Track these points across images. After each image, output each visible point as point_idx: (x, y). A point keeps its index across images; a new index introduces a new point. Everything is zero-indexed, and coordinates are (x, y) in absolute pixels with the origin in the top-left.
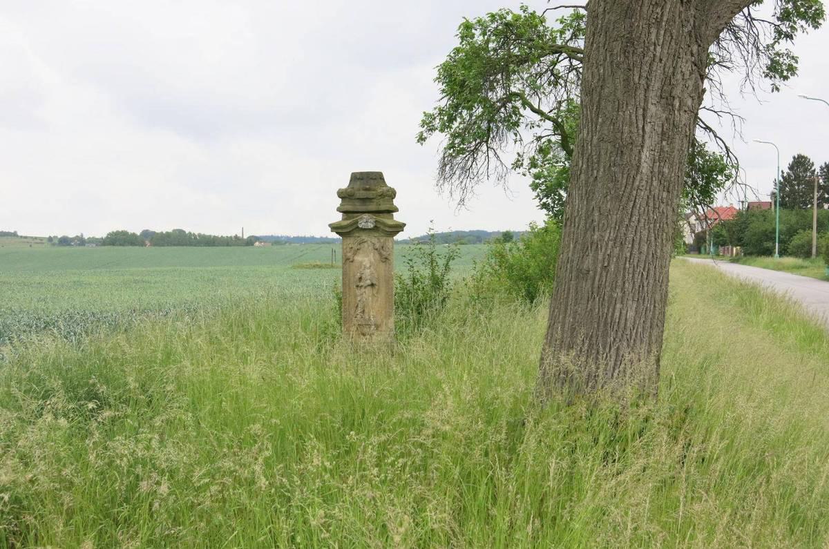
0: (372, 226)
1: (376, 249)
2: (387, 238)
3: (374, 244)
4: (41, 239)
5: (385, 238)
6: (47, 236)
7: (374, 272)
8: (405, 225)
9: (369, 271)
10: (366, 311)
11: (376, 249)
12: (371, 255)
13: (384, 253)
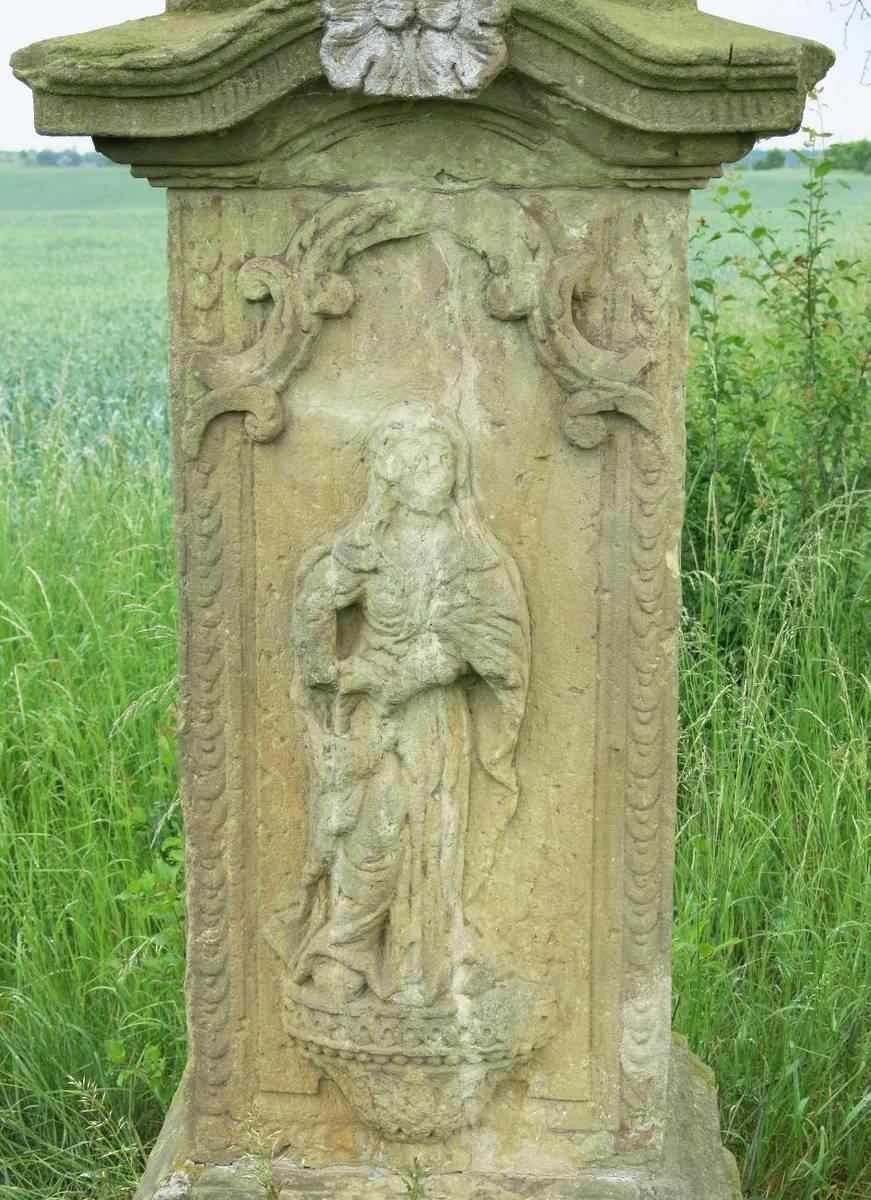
0: (473, 73)
1: (520, 319)
2: (627, 201)
3: (492, 268)
4: (9, 154)
5: (599, 206)
6: (19, 149)
7: (492, 549)
8: (819, 60)
9: (437, 536)
10: (407, 927)
11: (520, 319)
12: (465, 382)
13: (594, 360)
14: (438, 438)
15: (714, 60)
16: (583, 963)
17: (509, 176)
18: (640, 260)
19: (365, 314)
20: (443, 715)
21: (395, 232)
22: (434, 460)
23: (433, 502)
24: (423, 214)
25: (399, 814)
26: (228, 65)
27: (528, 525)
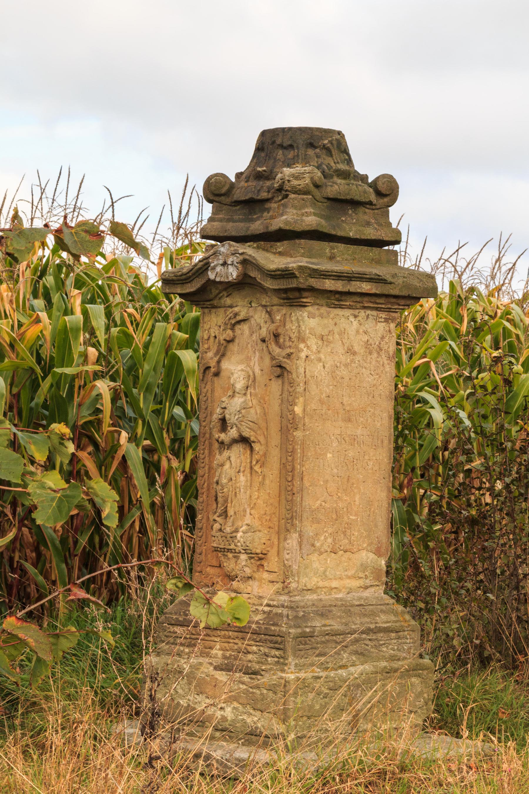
5: (284, 310)
9: (242, 400)
14: (243, 373)
15: (279, 270)
16: (276, 528)
17: (264, 303)
18: (291, 325)
19: (237, 341)
20: (241, 450)
21: (239, 318)
22: (241, 378)
23: (240, 390)
24: (247, 313)
25: (228, 476)
26: (194, 274)
27: (266, 398)
